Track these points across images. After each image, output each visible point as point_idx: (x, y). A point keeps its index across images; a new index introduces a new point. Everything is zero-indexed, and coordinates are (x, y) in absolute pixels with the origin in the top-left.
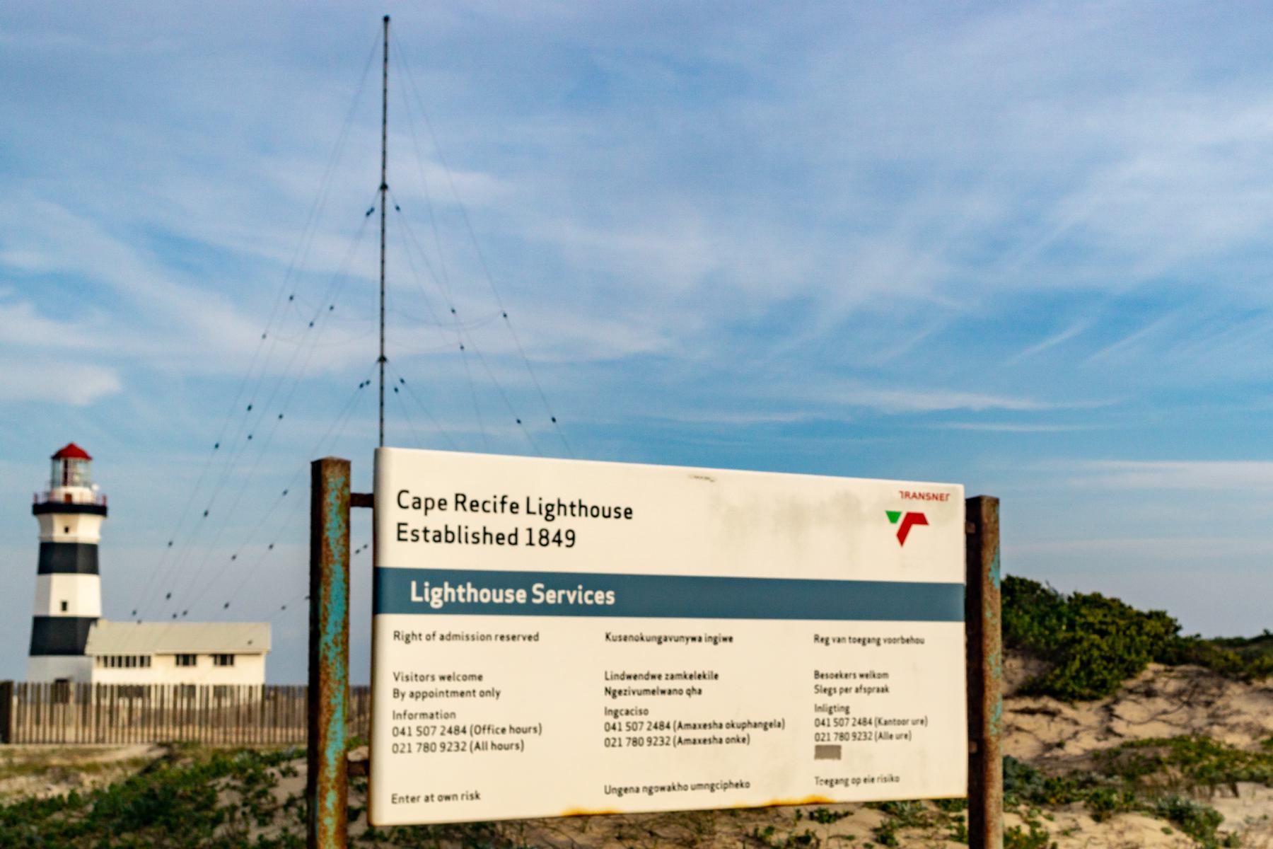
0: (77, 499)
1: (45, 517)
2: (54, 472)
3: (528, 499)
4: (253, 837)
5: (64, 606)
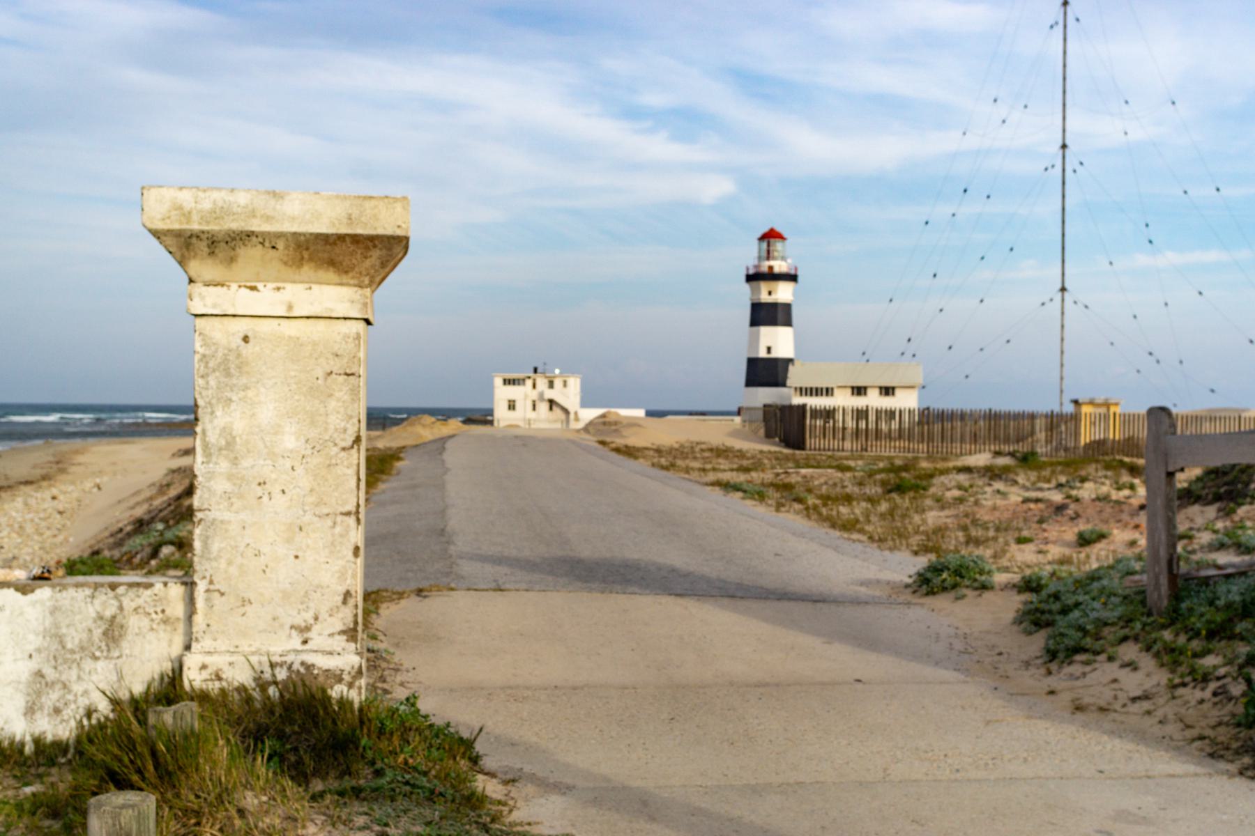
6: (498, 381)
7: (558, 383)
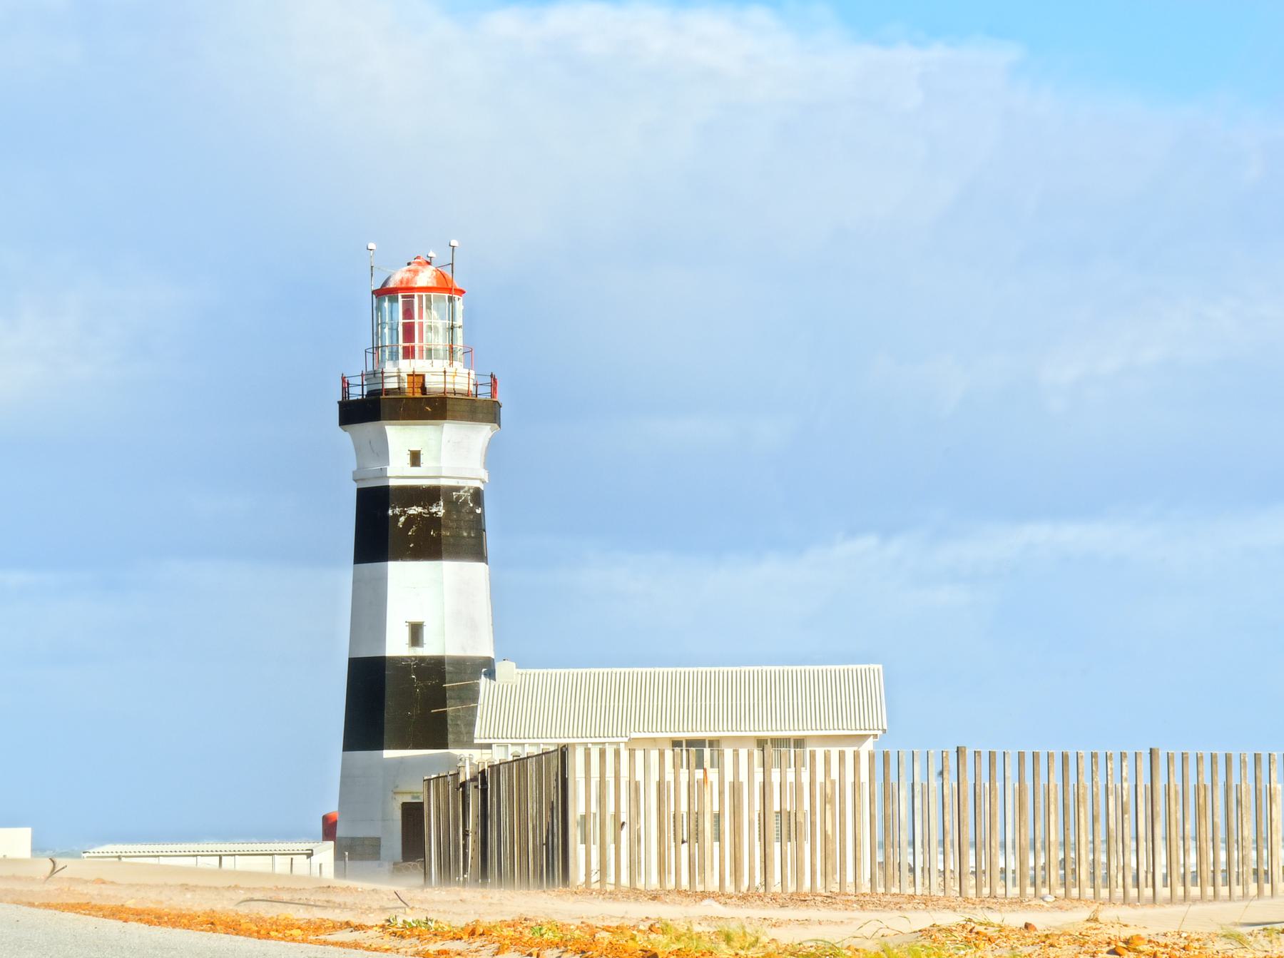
0: (434, 383)
1: (368, 428)
2: (377, 326)
3: (320, 865)
4: (1052, 955)
5: (416, 632)
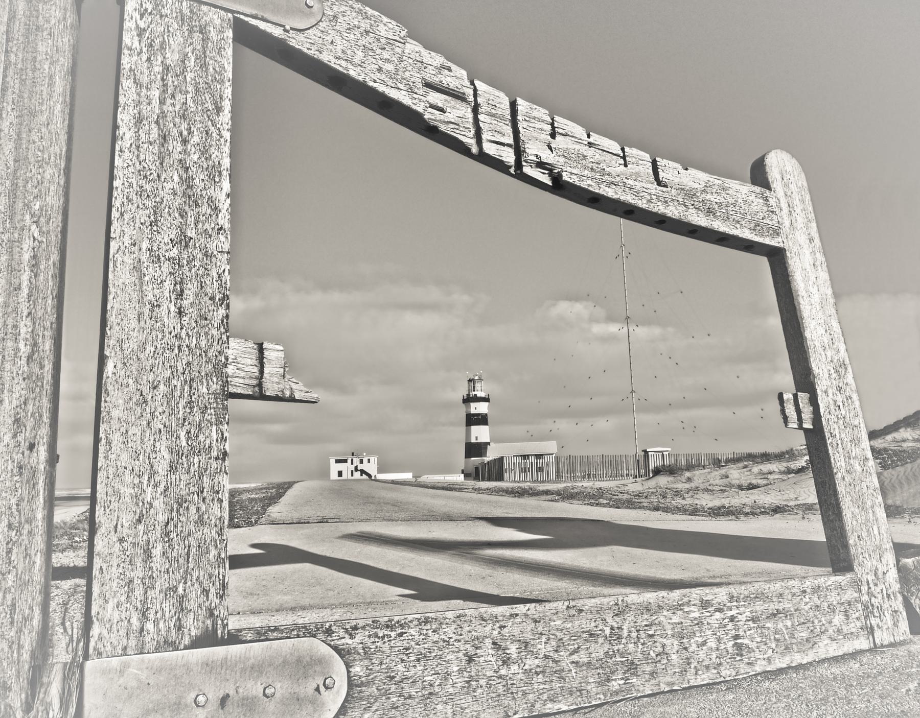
5: (477, 438)
6: (332, 461)
7: (365, 460)
